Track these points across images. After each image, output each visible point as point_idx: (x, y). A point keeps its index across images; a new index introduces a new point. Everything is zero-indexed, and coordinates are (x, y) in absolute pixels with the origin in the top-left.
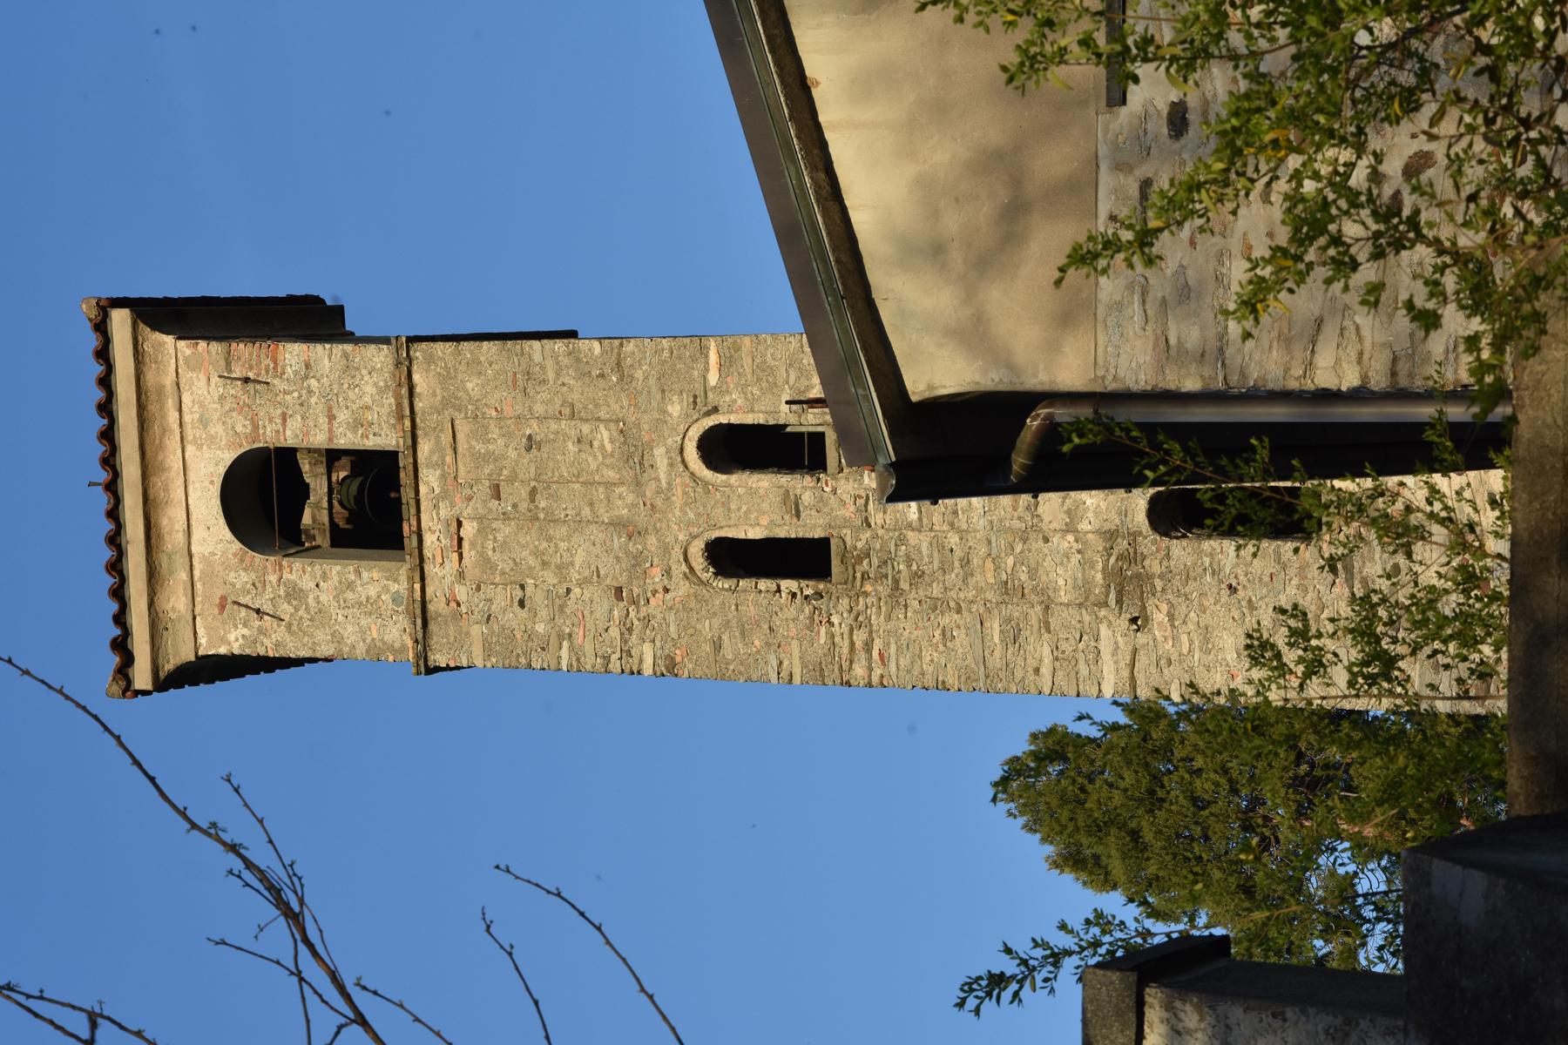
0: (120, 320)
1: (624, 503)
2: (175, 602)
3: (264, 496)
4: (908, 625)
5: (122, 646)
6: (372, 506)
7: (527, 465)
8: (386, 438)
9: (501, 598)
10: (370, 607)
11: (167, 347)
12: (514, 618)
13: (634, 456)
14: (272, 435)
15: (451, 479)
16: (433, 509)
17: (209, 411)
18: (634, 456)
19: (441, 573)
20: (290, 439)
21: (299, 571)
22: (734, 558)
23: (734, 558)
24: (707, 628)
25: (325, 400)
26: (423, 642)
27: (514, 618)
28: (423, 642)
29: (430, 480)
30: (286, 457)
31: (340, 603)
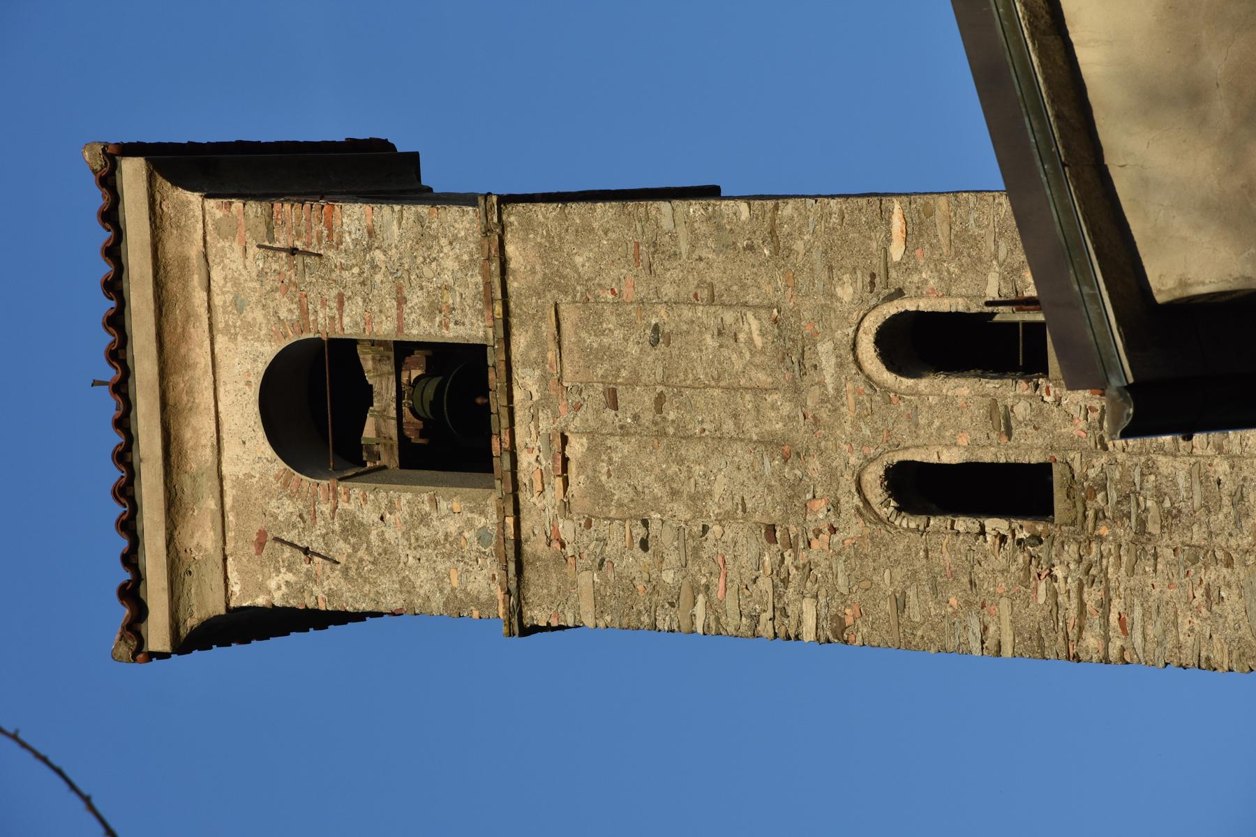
0: (132, 171)
1: (777, 415)
2: (201, 538)
3: (314, 403)
4: (1158, 582)
5: (132, 594)
6: (454, 417)
7: (652, 364)
8: (471, 328)
9: (618, 536)
10: (450, 547)
11: (193, 207)
12: (634, 564)
13: (792, 353)
14: (326, 323)
15: (553, 381)
16: (532, 414)
17: (244, 291)
18: (792, 353)
19: (540, 504)
20: (348, 327)
21: (358, 500)
22: (924, 489)
23: (924, 489)
24: (886, 581)
25: (393, 278)
26: (517, 593)
27: (634, 564)
28: (517, 593)
29: (527, 383)
30: (342, 353)
31: (412, 542)
